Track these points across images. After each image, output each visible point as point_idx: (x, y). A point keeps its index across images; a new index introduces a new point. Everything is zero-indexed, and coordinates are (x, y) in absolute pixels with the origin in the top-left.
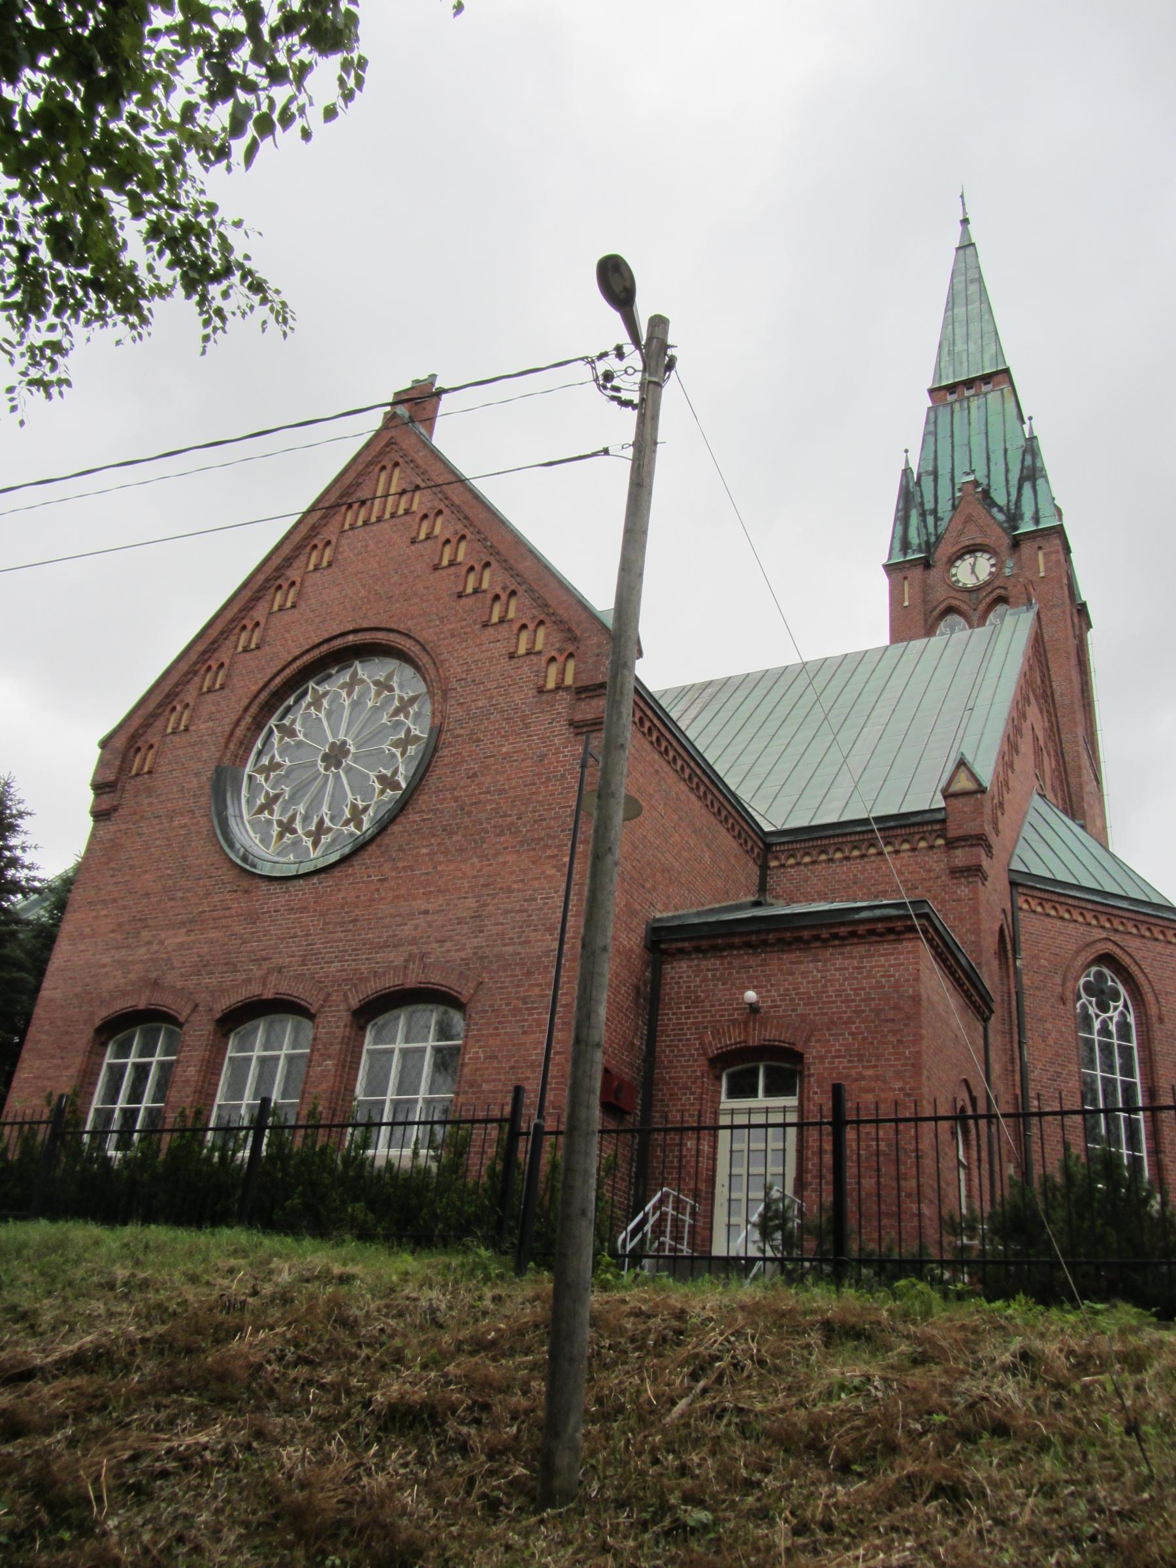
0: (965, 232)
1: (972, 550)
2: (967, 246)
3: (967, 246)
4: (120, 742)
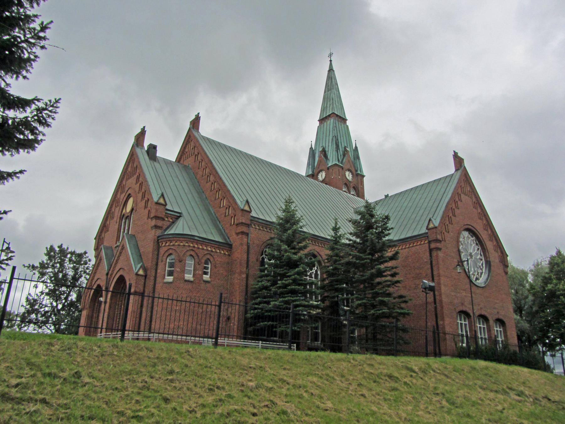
0: (331, 64)
1: (321, 171)
2: (331, 70)
3: (331, 70)
4: (505, 256)
